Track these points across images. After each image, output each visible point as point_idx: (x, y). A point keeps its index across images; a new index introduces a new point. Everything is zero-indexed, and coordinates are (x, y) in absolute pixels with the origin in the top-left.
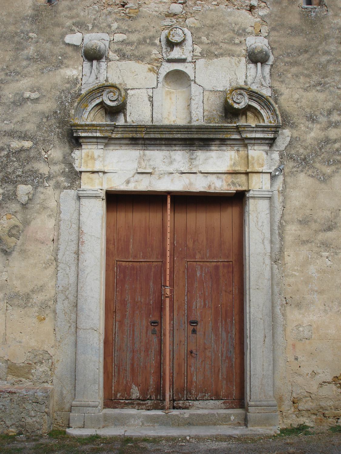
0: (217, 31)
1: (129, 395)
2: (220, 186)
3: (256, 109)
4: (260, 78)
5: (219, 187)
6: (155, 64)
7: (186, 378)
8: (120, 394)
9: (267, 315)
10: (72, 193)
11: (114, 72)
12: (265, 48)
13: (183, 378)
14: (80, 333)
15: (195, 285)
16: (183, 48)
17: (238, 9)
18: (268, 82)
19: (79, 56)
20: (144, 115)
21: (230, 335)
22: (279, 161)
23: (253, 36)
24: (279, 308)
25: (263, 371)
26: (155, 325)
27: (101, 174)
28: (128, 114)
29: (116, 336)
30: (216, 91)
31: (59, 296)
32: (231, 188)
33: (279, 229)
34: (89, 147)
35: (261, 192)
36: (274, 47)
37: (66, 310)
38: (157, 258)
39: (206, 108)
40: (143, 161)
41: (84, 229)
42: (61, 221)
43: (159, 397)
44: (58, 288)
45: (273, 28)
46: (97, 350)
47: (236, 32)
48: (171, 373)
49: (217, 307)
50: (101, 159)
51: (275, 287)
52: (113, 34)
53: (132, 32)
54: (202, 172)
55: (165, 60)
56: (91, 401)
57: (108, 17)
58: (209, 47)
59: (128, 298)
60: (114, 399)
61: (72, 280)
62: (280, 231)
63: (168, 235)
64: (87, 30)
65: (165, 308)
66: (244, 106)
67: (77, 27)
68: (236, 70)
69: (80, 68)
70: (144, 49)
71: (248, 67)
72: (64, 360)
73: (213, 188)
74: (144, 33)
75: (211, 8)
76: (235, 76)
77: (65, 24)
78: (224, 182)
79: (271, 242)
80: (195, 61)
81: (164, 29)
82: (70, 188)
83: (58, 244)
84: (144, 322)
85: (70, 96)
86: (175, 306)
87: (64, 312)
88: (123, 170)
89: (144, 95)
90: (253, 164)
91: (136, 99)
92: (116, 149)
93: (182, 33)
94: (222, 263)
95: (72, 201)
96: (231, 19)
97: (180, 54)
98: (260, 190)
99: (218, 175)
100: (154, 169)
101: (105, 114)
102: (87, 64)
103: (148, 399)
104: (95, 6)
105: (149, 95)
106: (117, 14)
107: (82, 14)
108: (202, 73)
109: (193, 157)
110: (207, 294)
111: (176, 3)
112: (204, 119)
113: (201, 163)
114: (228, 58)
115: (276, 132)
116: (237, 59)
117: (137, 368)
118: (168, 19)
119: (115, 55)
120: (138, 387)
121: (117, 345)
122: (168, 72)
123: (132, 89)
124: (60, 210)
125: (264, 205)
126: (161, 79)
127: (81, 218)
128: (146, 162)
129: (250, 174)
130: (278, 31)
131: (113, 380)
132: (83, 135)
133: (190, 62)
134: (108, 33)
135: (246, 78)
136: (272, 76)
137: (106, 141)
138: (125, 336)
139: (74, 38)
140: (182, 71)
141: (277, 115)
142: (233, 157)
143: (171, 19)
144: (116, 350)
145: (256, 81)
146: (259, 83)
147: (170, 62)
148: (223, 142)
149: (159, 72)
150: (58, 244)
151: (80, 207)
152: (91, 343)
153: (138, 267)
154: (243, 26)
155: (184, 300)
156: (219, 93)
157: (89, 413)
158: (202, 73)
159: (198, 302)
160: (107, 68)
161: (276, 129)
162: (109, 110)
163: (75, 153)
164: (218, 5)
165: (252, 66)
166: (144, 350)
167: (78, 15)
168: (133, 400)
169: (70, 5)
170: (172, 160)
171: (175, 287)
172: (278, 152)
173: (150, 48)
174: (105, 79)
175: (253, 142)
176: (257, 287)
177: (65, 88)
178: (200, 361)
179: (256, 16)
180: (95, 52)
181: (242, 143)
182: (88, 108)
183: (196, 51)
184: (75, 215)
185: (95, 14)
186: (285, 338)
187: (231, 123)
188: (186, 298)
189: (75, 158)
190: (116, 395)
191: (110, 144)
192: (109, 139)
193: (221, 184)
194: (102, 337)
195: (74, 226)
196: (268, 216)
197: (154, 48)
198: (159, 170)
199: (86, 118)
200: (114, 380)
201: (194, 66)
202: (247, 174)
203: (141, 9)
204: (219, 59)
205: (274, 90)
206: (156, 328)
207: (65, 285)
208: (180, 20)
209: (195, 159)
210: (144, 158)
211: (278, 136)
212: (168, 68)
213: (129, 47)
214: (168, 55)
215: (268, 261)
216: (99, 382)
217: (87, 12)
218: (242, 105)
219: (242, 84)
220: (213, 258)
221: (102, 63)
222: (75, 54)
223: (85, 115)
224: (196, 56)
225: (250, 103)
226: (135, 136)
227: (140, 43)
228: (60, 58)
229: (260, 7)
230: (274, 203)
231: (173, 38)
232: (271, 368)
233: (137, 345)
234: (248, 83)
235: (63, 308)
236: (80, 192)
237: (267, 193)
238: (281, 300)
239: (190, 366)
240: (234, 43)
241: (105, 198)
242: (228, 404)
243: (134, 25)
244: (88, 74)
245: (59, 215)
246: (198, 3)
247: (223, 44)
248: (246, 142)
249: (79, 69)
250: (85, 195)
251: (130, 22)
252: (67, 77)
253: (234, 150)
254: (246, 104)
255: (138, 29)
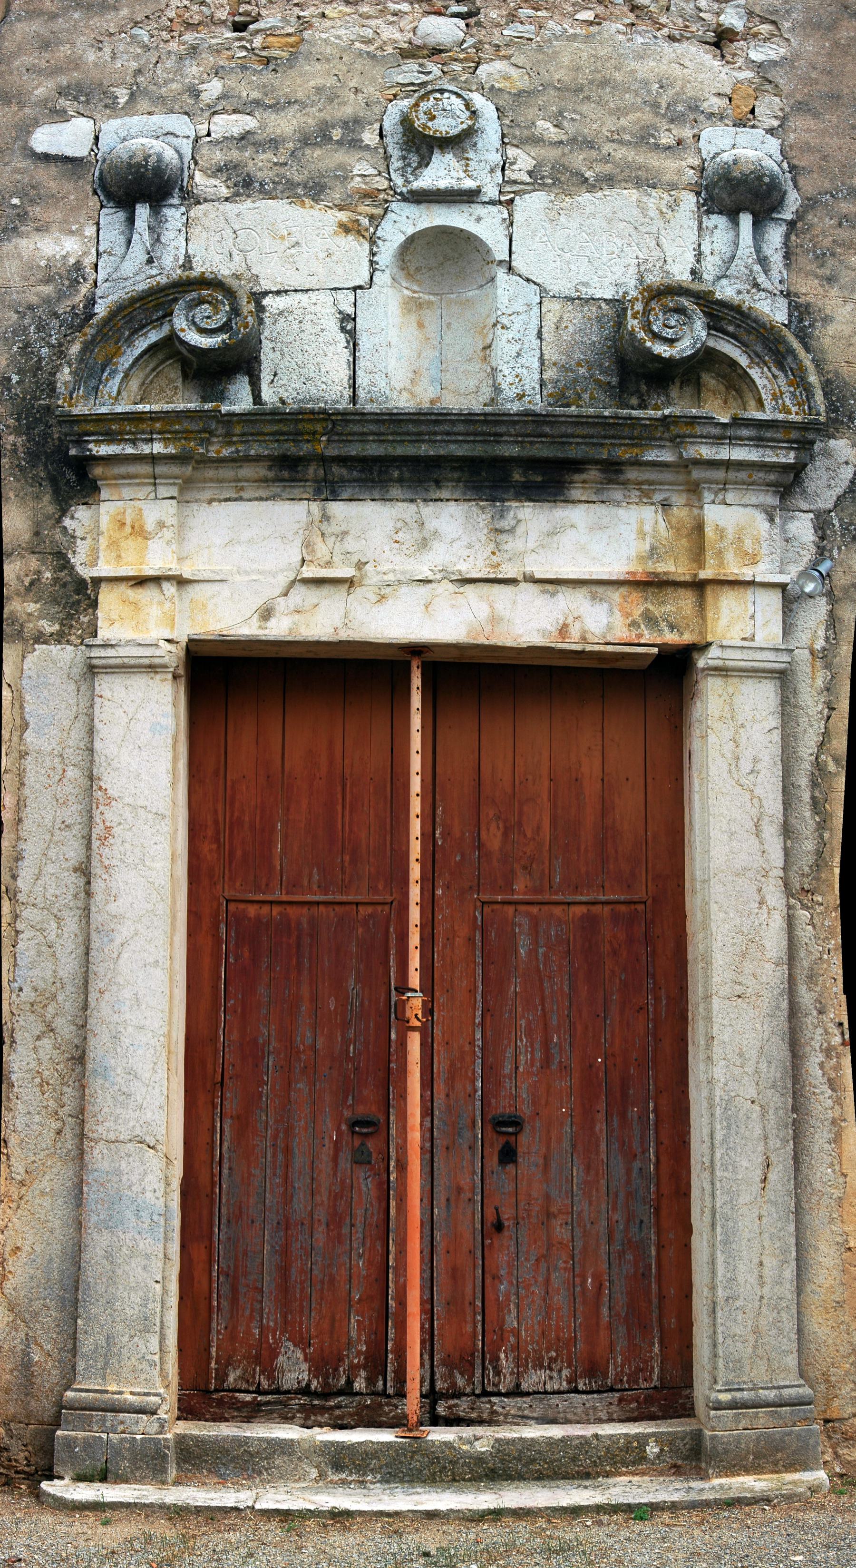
0: (593, 105)
1: (270, 1371)
2: (600, 625)
3: (734, 364)
4: (750, 261)
5: (597, 632)
6: (362, 208)
7: (479, 1318)
8: (238, 1372)
9: (774, 1086)
10: (66, 655)
11: (212, 237)
12: (770, 165)
13: (469, 1318)
14: (99, 1157)
15: (512, 989)
16: (466, 155)
17: (672, 38)
18: (776, 276)
19: (80, 192)
20: (324, 379)
21: (637, 1165)
22: (812, 545)
23: (727, 125)
24: (818, 1060)
25: (762, 1285)
26: (365, 1130)
27: (170, 589)
28: (265, 377)
29: (225, 1171)
30: (587, 301)
31: (22, 1023)
32: (640, 636)
33: (814, 784)
34: (126, 492)
35: (750, 652)
36: (802, 164)
37: (47, 1073)
38: (373, 889)
39: (551, 354)
40: (320, 539)
41: (111, 782)
42: (29, 758)
43: (381, 1383)
44: (18, 996)
45: (800, 103)
46: (155, 1218)
47: (663, 112)
48: (426, 1301)
49: (591, 1066)
50: (168, 534)
51: (802, 989)
52: (207, 114)
53: (275, 107)
54: (538, 576)
55: (401, 194)
56: (132, 1393)
57: (187, 62)
58: (564, 155)
59: (267, 1032)
60: (217, 1391)
61: (68, 965)
62: (817, 794)
63: (416, 806)
64: (112, 107)
65: (403, 1095)
66: (689, 352)
67: (76, 99)
68: (663, 232)
69: (90, 231)
70: (323, 159)
71: (704, 226)
72: (38, 1248)
73: (575, 632)
74: (320, 110)
75: (571, 31)
76: (657, 253)
77: (31, 93)
78: (618, 614)
79: (787, 831)
80: (512, 201)
81: (395, 96)
82: (60, 638)
83: (19, 838)
84: (328, 1123)
85: (55, 323)
86: (439, 1063)
87: (38, 1080)
88: (247, 573)
89: (324, 312)
90: (720, 554)
91: (295, 326)
92: (222, 497)
93: (463, 108)
94: (607, 909)
95: (64, 687)
96: (646, 69)
97: (454, 174)
98: (746, 644)
99: (594, 588)
100: (360, 565)
101: (184, 381)
102: (112, 220)
103: (340, 1393)
104: (136, 31)
105: (340, 312)
106: (218, 52)
107: (91, 56)
108: (537, 239)
109: (505, 524)
110: (555, 1022)
111: (440, 14)
112: (545, 393)
113: (531, 545)
114: (632, 194)
115: (804, 446)
116: (665, 196)
117: (302, 1282)
118: (412, 65)
119: (216, 182)
120: (304, 1350)
121: (228, 1201)
122: (410, 231)
123: (278, 293)
124: (23, 718)
125: (758, 700)
126: (387, 254)
127: (98, 745)
128: (331, 541)
129: (709, 591)
130: (816, 116)
131: (214, 1325)
132: (104, 450)
133: (492, 203)
134: (186, 113)
135: (698, 261)
136: (793, 258)
137: (188, 470)
138: (256, 1172)
139: (68, 137)
140: (462, 230)
141: (808, 389)
142: (648, 528)
143: (421, 65)
144: (224, 1220)
145: (732, 271)
146: (744, 278)
147: (418, 202)
148: (613, 472)
149: (379, 234)
150: (19, 838)
151: (92, 706)
152: (133, 1188)
153: (304, 921)
154: (690, 93)
155: (472, 1043)
156: (600, 307)
157: (123, 1432)
158: (537, 239)
159: (523, 1050)
160: (187, 225)
161: (805, 437)
162: (195, 366)
163: (76, 516)
164: (599, 24)
165: (719, 221)
166: (324, 1220)
167: (75, 63)
168: (288, 1392)
169: (44, 31)
170: (427, 536)
171: (437, 994)
172: (811, 515)
173: (340, 156)
174: (181, 262)
175: (720, 474)
176: (739, 990)
177: (34, 300)
178: (533, 1259)
179: (738, 65)
180: (143, 175)
181: (681, 478)
182: (121, 360)
183: (515, 167)
184: (77, 735)
185: (137, 57)
186: (837, 1168)
187: (643, 406)
188: (478, 1035)
189: (77, 534)
190: (222, 1376)
191: (200, 482)
192: (198, 462)
193: (605, 621)
194: (177, 1171)
195: (71, 773)
196: (776, 736)
197: (357, 157)
198: (379, 569)
199: (114, 394)
200: (218, 1324)
201: (506, 215)
202: (699, 586)
203: (307, 34)
204: (599, 194)
205: (798, 307)
206: (370, 1144)
207: (41, 985)
208: (457, 67)
209: (512, 531)
210: (324, 526)
211: (812, 458)
212: (410, 221)
213: (269, 155)
214: (411, 178)
215: (775, 898)
216: (162, 1327)
217: (107, 50)
218: (684, 348)
219: (680, 273)
220: (576, 890)
221: (168, 212)
222: (69, 186)
223: (110, 383)
224: (515, 182)
225: (711, 343)
226: (292, 449)
227: (306, 141)
228: (15, 201)
229: (755, 35)
230: (795, 692)
231: (430, 124)
232: (789, 1272)
233: (300, 1205)
234: (705, 276)
235: (33, 1065)
236: (95, 653)
237: (771, 656)
238: (827, 1032)
239: (496, 1277)
240: (657, 146)
241: (181, 671)
242: (634, 1405)
243: (289, 84)
244: (119, 250)
245: (21, 737)
246: (522, 16)
247: (615, 146)
248: (697, 474)
249: (87, 234)
250: (112, 662)
251: (268, 77)
252: (43, 263)
253: (652, 504)
254: (698, 346)
255: (300, 95)
